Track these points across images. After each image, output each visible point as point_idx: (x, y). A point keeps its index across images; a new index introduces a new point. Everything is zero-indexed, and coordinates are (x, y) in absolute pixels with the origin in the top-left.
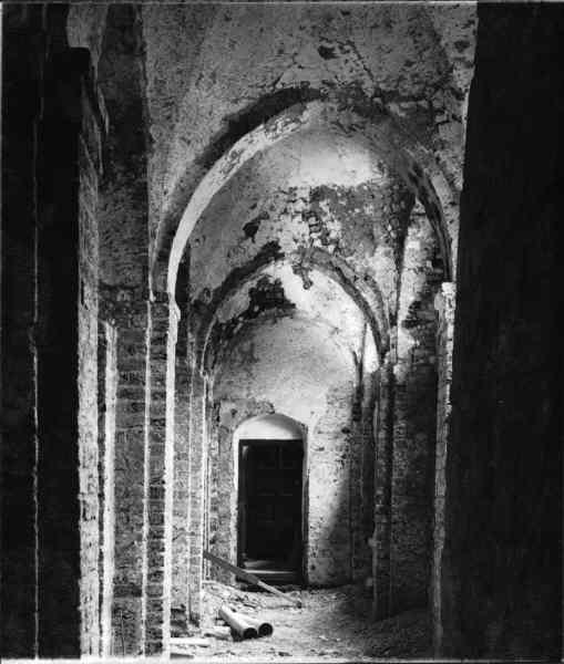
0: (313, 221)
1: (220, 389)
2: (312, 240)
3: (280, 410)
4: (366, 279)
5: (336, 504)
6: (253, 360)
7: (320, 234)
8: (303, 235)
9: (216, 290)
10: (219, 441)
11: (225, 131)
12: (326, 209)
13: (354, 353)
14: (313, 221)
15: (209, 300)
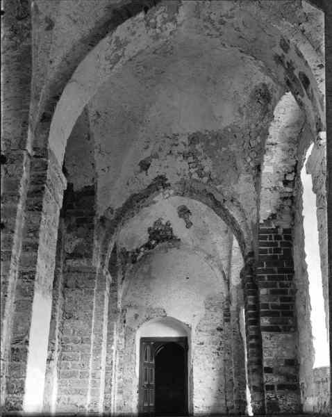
0: (191, 159)
1: (127, 298)
2: (191, 174)
3: (171, 314)
4: (232, 201)
5: (215, 388)
6: (151, 278)
7: (197, 169)
8: (184, 170)
9: (118, 210)
10: (125, 338)
11: (109, 17)
12: (201, 150)
13: (223, 272)
14: (191, 159)
15: (112, 217)
